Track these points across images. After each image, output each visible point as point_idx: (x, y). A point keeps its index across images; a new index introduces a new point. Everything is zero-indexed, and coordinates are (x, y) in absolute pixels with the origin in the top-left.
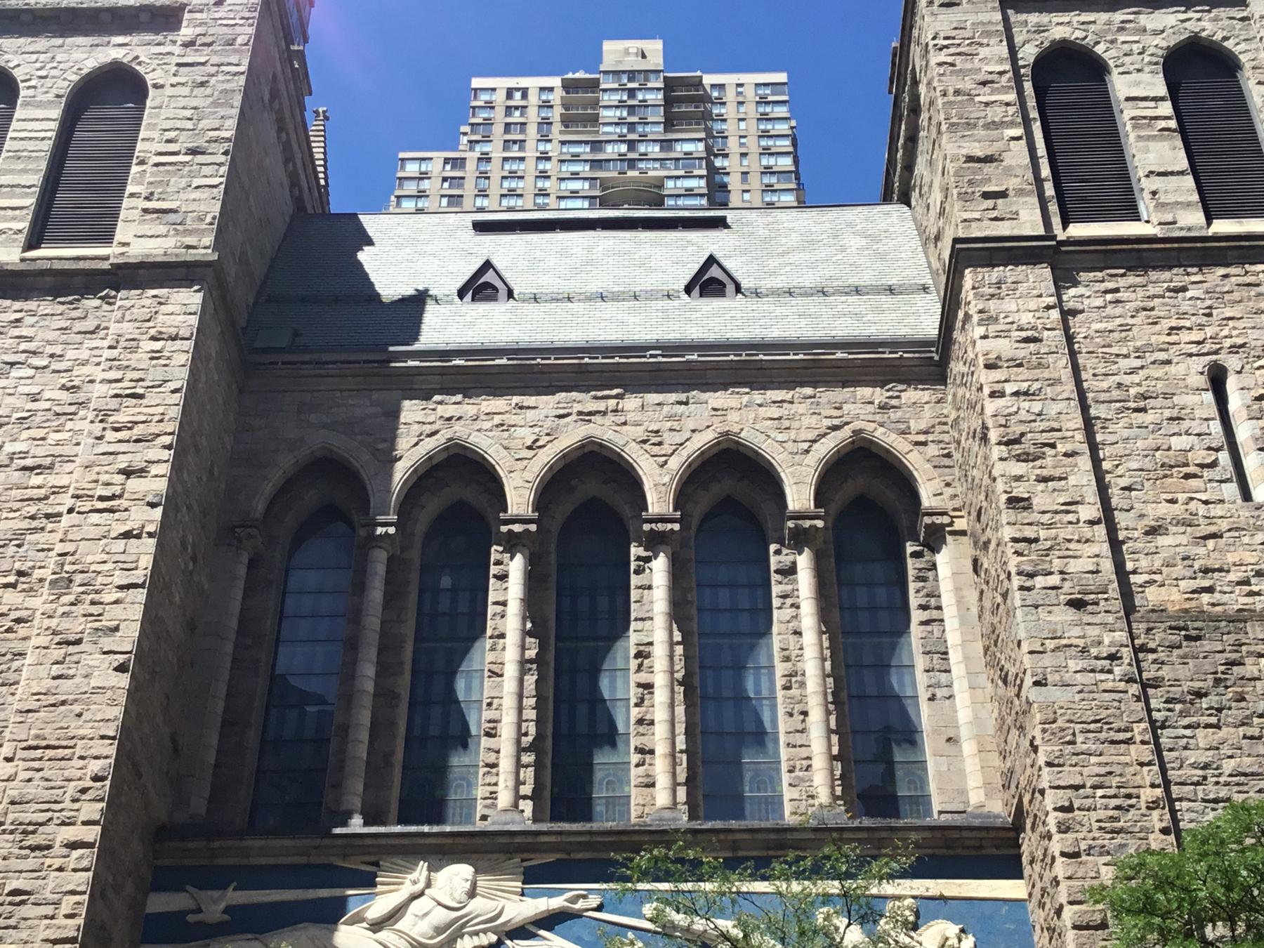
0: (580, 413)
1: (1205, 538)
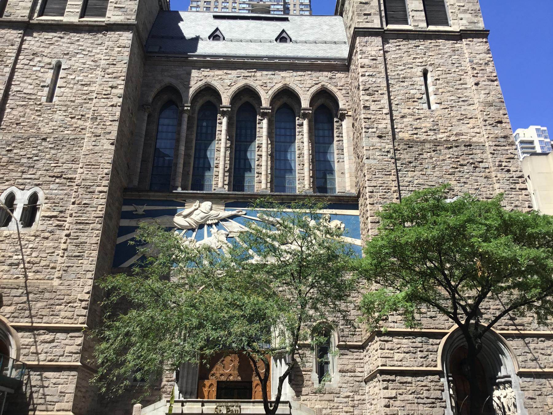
0: (244, 76)
1: (417, 119)
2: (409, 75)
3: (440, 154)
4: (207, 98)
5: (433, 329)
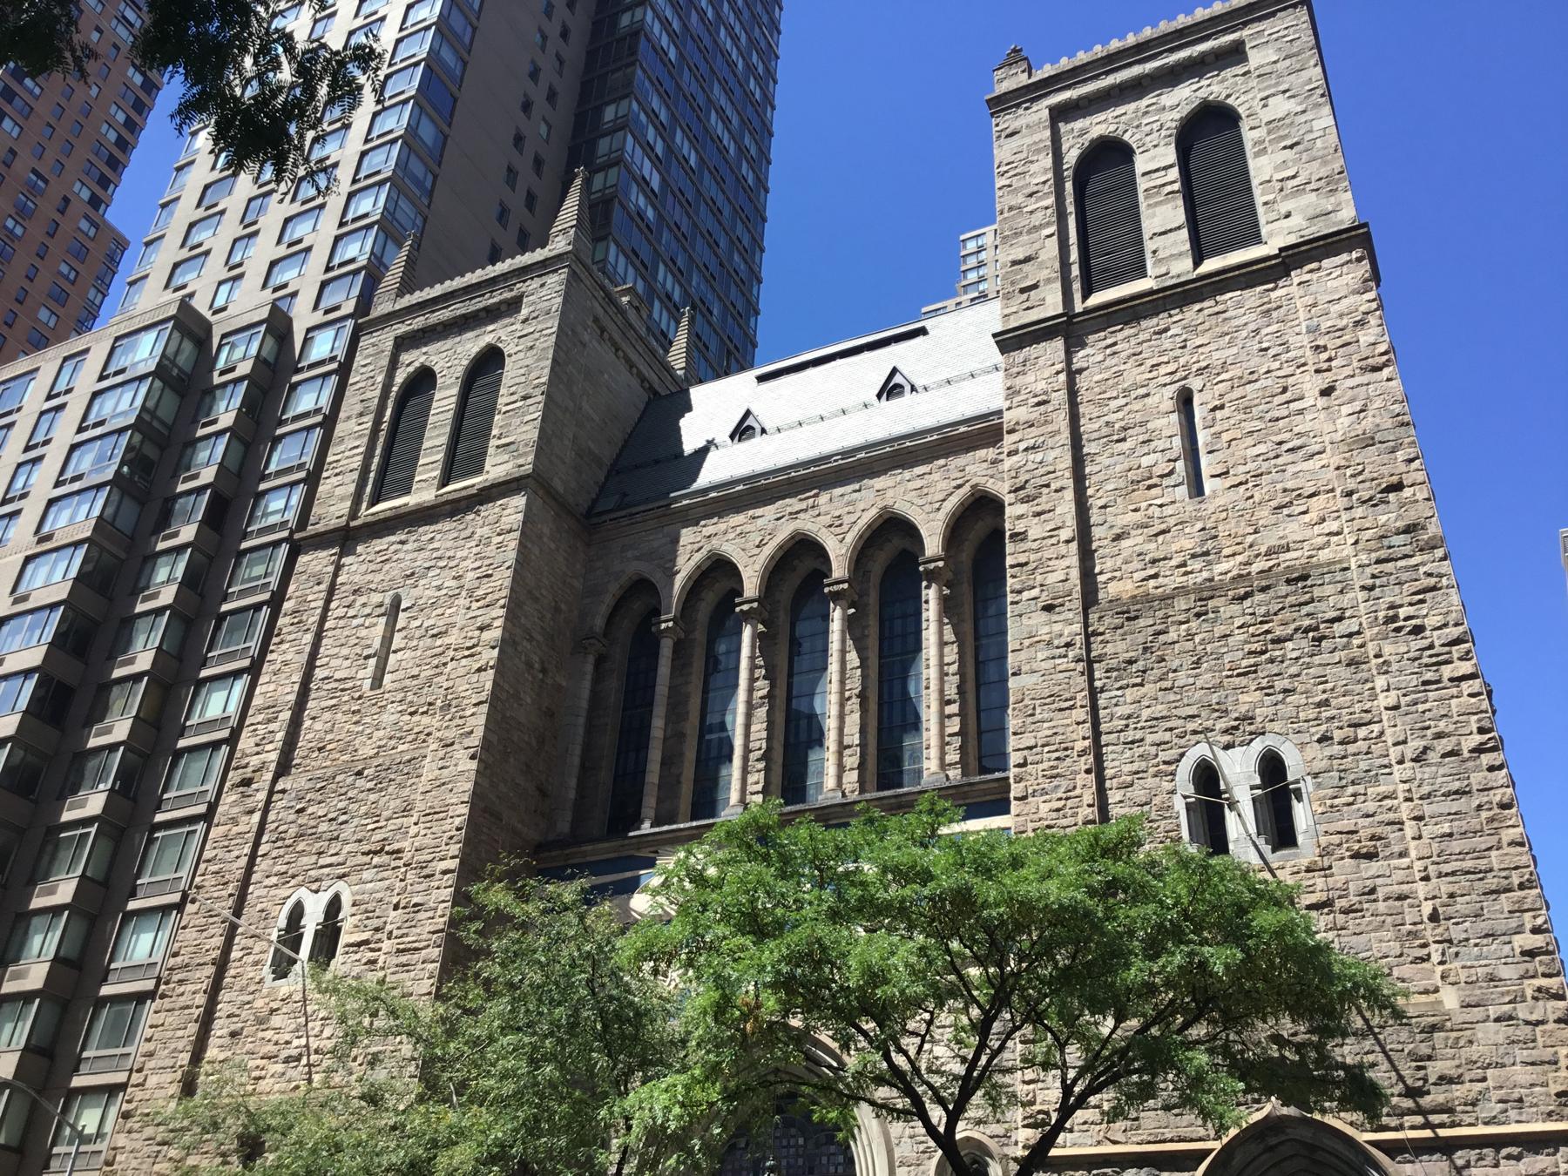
0: (791, 514)
1: (1156, 535)
2: (1138, 418)
3: (1215, 620)
4: (897, 543)
5: (1172, 1141)
